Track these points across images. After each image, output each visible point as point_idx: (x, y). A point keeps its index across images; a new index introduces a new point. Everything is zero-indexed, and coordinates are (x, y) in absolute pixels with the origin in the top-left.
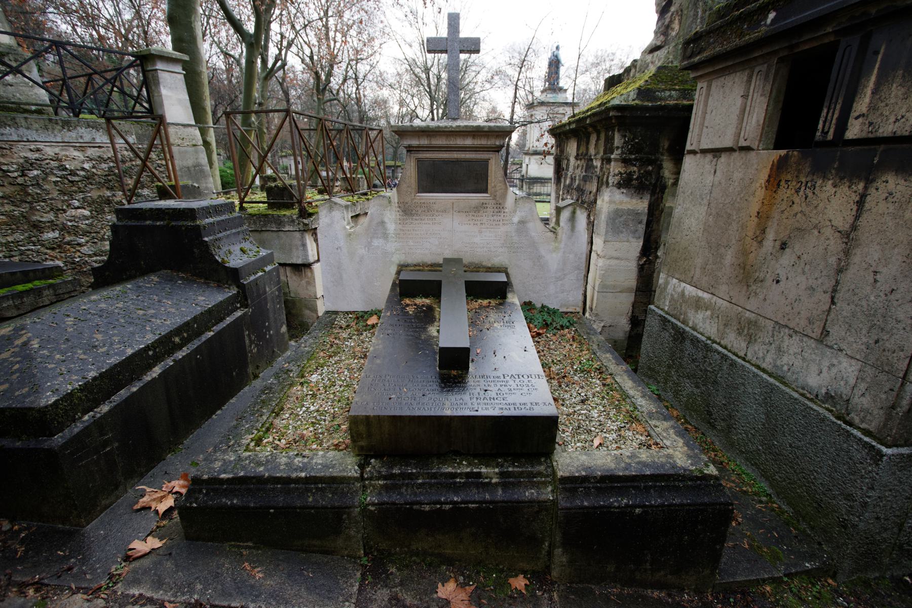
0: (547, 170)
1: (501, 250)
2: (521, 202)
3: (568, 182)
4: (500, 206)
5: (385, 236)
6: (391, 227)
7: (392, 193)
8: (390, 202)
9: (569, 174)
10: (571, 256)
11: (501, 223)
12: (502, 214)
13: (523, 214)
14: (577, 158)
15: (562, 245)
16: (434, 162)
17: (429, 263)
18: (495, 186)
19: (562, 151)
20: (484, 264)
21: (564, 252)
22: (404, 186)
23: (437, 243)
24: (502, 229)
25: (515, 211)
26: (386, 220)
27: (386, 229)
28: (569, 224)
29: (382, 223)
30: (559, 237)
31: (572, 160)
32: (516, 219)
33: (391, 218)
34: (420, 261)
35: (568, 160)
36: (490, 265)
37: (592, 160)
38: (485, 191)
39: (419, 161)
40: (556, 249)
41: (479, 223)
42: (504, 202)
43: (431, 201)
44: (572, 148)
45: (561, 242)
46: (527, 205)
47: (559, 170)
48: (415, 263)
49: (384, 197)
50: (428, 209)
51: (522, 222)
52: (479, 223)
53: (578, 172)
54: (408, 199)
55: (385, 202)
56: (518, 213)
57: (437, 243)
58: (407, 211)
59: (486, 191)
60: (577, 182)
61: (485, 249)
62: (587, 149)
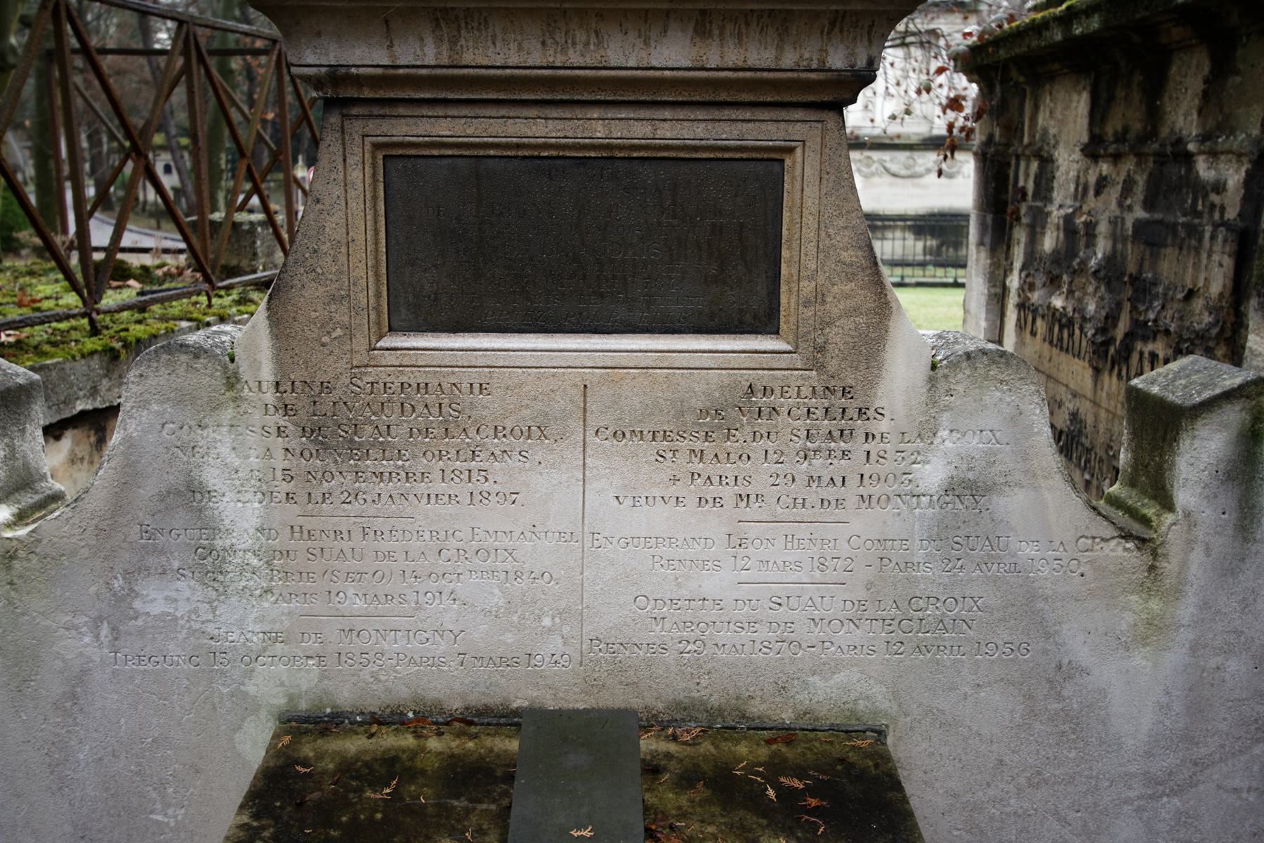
0: (957, 188)
1: (847, 635)
2: (960, 381)
3: (1049, 243)
4: (843, 403)
5: (209, 563)
6: (241, 515)
7: (248, 335)
8: (233, 382)
9: (1056, 214)
10: (1236, 666)
11: (851, 492)
12: (858, 447)
13: (974, 444)
14: (1093, 150)
15: (1186, 610)
16: (476, 162)
17: (456, 705)
18: (820, 297)
19: (1012, 130)
20: (756, 708)
21: (1194, 648)
22: (309, 296)
23: (498, 599)
24: (862, 525)
25: (928, 431)
26: (212, 477)
27: (211, 527)
28: (1228, 499)
29: (191, 495)
30: (1169, 566)
31: (1068, 162)
32: (932, 474)
33: (239, 466)
34: (402, 693)
35: (1047, 162)
36: (787, 717)
37: (1188, 158)
38: (764, 320)
39: (393, 158)
40: (1153, 630)
41: (728, 492)
42: (871, 383)
43: (465, 377)
44: (1065, 118)
45: (1177, 592)
46: (994, 395)
47: (1001, 200)
48: (373, 706)
49: (197, 352)
50: (447, 421)
51: (968, 489)
52: (728, 492)
53: (1105, 208)
54: (333, 367)
55: (206, 379)
56: (947, 442)
57: (498, 599)
58: (329, 429)
59: (766, 322)
60: (1102, 248)
61: (763, 633)
62: (1154, 115)
